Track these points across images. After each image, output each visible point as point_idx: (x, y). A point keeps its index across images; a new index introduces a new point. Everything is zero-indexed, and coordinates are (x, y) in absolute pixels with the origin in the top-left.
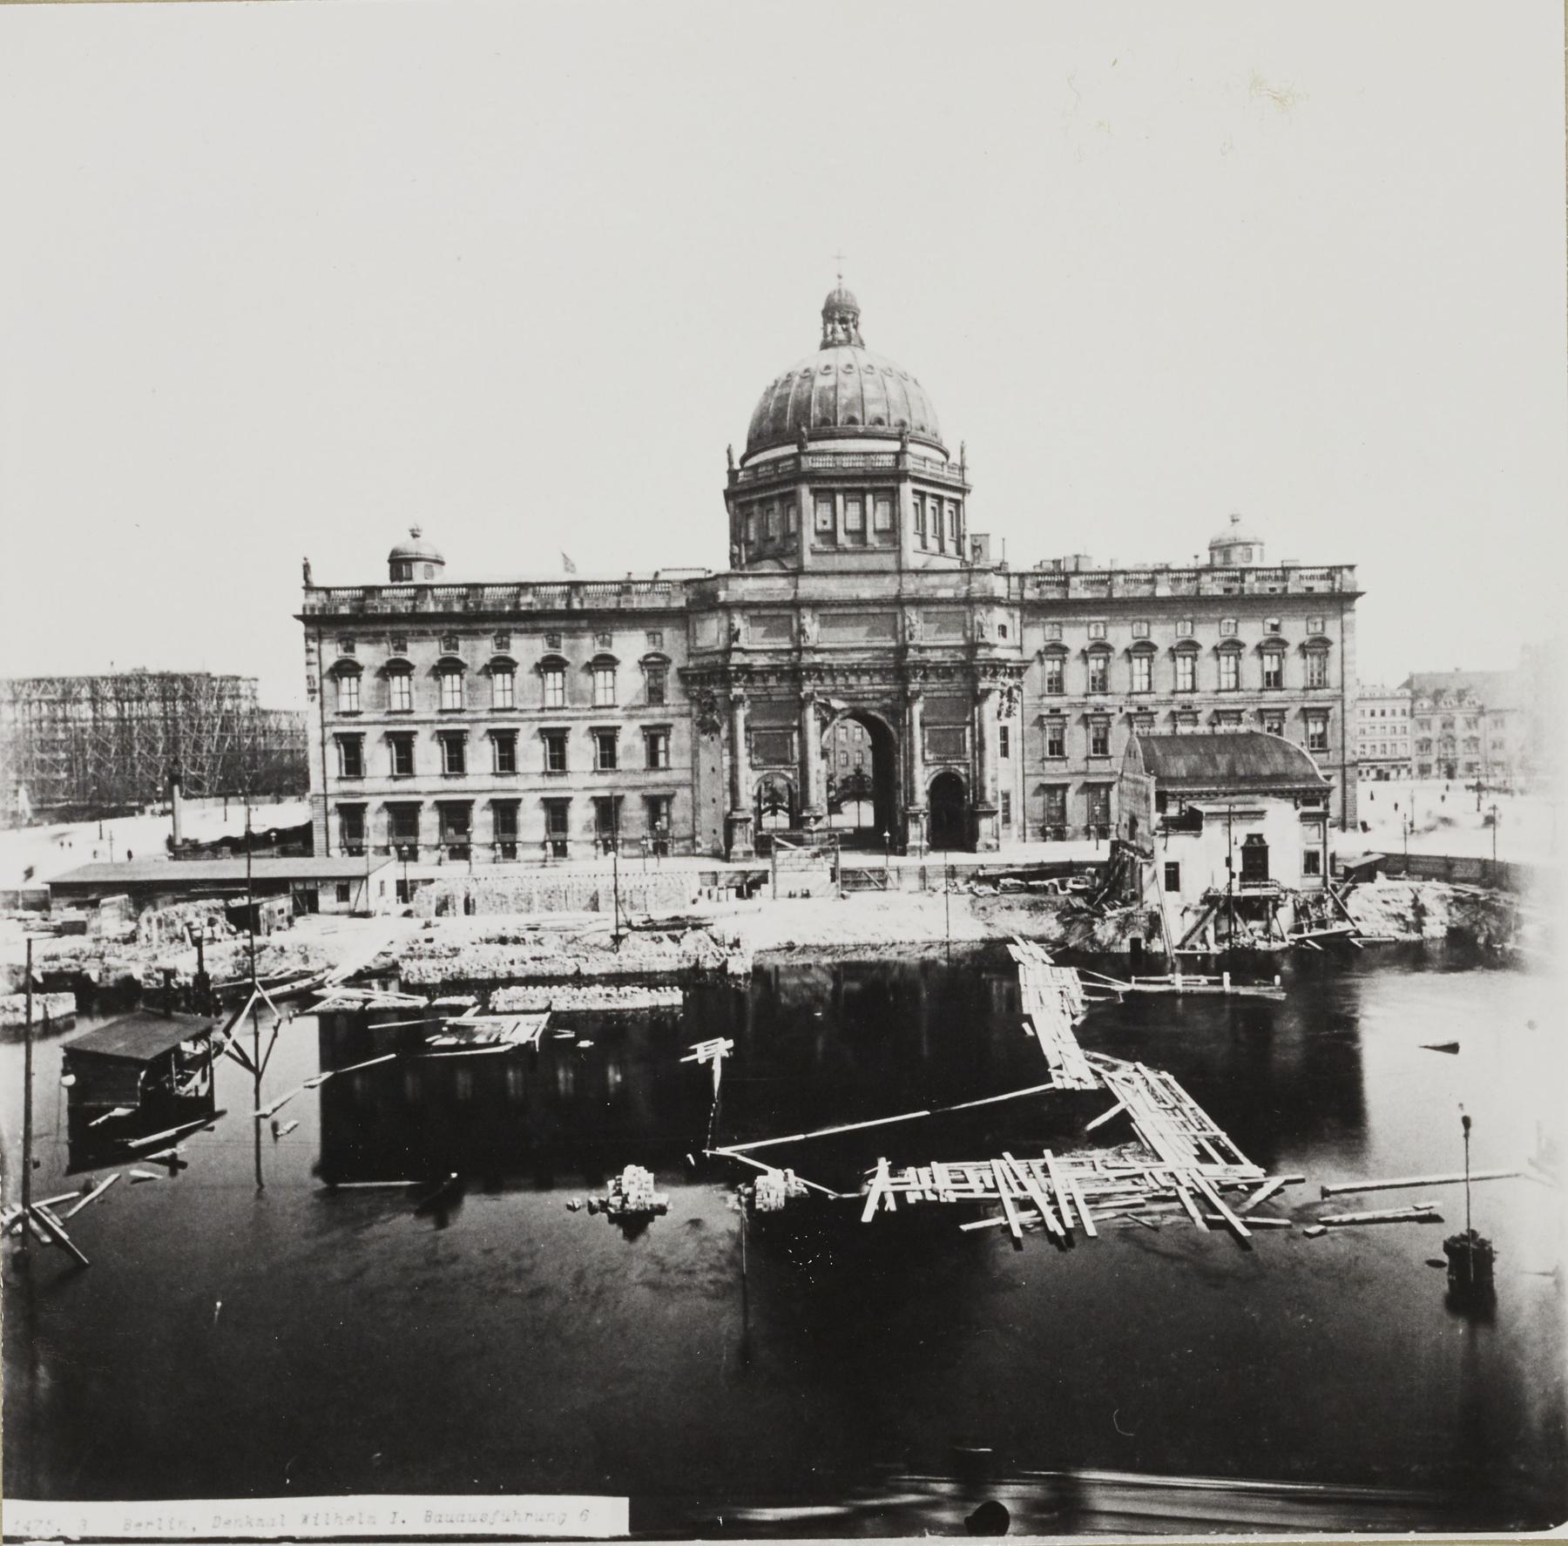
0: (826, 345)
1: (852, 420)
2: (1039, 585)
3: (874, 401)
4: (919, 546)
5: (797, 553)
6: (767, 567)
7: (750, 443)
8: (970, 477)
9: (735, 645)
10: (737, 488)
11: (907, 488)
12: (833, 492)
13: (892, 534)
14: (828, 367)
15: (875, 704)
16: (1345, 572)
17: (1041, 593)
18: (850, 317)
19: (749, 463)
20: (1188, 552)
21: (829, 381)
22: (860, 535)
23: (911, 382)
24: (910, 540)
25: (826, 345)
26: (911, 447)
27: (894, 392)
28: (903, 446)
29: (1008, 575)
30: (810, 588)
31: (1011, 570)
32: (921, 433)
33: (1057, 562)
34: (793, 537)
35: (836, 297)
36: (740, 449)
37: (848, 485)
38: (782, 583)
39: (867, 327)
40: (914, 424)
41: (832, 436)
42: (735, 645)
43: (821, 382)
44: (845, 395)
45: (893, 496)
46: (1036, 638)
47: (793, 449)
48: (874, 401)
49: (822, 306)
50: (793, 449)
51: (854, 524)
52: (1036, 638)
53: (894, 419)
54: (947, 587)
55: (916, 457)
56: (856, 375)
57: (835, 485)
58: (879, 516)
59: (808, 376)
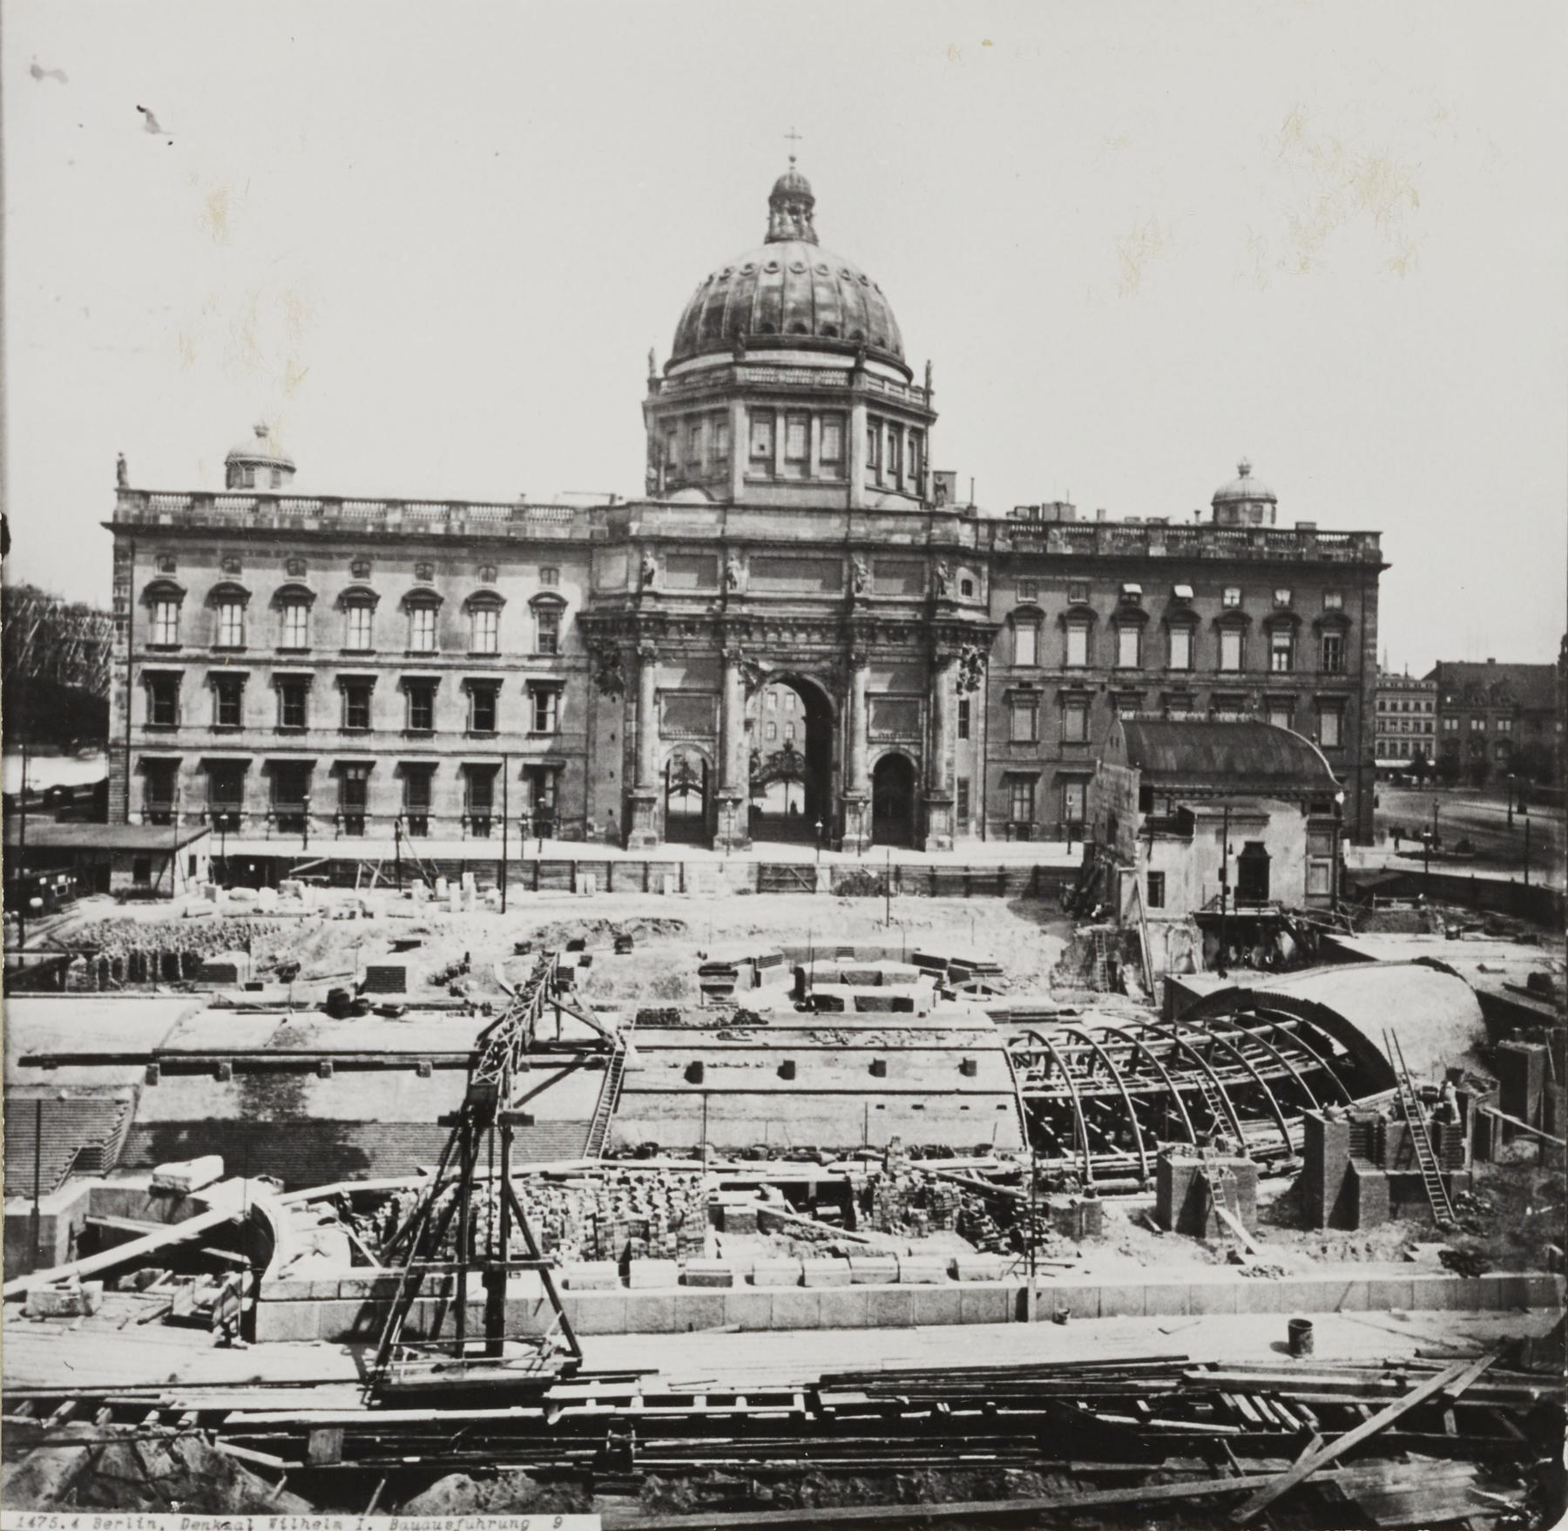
0: (771, 239)
1: (800, 328)
2: (1012, 535)
3: (825, 307)
4: (872, 482)
5: (726, 481)
6: (694, 496)
7: (676, 349)
8: (936, 404)
9: (646, 588)
10: (660, 399)
11: (860, 413)
12: (772, 412)
13: (842, 464)
14: (773, 264)
15: (811, 667)
16: (1369, 540)
17: (1015, 545)
18: (802, 207)
19: (674, 372)
20: (1186, 504)
21: (775, 280)
22: (803, 463)
23: (871, 289)
24: (861, 476)
25: (771, 239)
26: (870, 365)
27: (849, 296)
28: (858, 362)
29: (976, 523)
30: (741, 525)
31: (981, 515)
32: (880, 349)
33: (1034, 510)
34: (723, 462)
35: (787, 184)
36: (665, 353)
37: (790, 404)
38: (711, 517)
39: (823, 217)
40: (873, 338)
41: (777, 345)
42: (646, 588)
43: (765, 280)
44: (796, 296)
45: (844, 418)
46: (1007, 600)
47: (727, 358)
48: (825, 307)
49: (769, 192)
50: (727, 358)
51: (796, 451)
52: (1007, 600)
53: (850, 328)
54: (902, 532)
55: (873, 375)
56: (806, 276)
57: (779, 404)
58: (826, 444)
59: (750, 273)
